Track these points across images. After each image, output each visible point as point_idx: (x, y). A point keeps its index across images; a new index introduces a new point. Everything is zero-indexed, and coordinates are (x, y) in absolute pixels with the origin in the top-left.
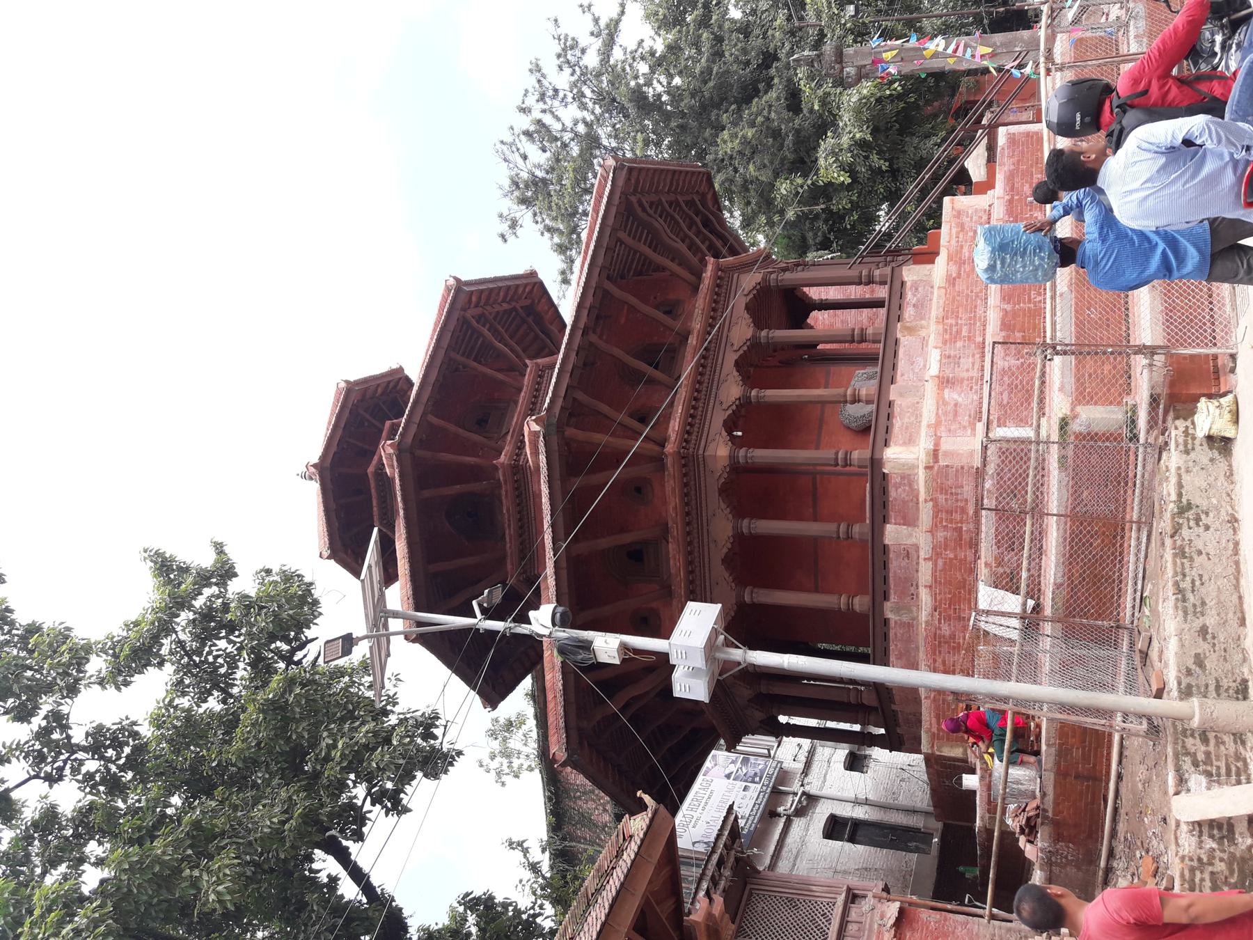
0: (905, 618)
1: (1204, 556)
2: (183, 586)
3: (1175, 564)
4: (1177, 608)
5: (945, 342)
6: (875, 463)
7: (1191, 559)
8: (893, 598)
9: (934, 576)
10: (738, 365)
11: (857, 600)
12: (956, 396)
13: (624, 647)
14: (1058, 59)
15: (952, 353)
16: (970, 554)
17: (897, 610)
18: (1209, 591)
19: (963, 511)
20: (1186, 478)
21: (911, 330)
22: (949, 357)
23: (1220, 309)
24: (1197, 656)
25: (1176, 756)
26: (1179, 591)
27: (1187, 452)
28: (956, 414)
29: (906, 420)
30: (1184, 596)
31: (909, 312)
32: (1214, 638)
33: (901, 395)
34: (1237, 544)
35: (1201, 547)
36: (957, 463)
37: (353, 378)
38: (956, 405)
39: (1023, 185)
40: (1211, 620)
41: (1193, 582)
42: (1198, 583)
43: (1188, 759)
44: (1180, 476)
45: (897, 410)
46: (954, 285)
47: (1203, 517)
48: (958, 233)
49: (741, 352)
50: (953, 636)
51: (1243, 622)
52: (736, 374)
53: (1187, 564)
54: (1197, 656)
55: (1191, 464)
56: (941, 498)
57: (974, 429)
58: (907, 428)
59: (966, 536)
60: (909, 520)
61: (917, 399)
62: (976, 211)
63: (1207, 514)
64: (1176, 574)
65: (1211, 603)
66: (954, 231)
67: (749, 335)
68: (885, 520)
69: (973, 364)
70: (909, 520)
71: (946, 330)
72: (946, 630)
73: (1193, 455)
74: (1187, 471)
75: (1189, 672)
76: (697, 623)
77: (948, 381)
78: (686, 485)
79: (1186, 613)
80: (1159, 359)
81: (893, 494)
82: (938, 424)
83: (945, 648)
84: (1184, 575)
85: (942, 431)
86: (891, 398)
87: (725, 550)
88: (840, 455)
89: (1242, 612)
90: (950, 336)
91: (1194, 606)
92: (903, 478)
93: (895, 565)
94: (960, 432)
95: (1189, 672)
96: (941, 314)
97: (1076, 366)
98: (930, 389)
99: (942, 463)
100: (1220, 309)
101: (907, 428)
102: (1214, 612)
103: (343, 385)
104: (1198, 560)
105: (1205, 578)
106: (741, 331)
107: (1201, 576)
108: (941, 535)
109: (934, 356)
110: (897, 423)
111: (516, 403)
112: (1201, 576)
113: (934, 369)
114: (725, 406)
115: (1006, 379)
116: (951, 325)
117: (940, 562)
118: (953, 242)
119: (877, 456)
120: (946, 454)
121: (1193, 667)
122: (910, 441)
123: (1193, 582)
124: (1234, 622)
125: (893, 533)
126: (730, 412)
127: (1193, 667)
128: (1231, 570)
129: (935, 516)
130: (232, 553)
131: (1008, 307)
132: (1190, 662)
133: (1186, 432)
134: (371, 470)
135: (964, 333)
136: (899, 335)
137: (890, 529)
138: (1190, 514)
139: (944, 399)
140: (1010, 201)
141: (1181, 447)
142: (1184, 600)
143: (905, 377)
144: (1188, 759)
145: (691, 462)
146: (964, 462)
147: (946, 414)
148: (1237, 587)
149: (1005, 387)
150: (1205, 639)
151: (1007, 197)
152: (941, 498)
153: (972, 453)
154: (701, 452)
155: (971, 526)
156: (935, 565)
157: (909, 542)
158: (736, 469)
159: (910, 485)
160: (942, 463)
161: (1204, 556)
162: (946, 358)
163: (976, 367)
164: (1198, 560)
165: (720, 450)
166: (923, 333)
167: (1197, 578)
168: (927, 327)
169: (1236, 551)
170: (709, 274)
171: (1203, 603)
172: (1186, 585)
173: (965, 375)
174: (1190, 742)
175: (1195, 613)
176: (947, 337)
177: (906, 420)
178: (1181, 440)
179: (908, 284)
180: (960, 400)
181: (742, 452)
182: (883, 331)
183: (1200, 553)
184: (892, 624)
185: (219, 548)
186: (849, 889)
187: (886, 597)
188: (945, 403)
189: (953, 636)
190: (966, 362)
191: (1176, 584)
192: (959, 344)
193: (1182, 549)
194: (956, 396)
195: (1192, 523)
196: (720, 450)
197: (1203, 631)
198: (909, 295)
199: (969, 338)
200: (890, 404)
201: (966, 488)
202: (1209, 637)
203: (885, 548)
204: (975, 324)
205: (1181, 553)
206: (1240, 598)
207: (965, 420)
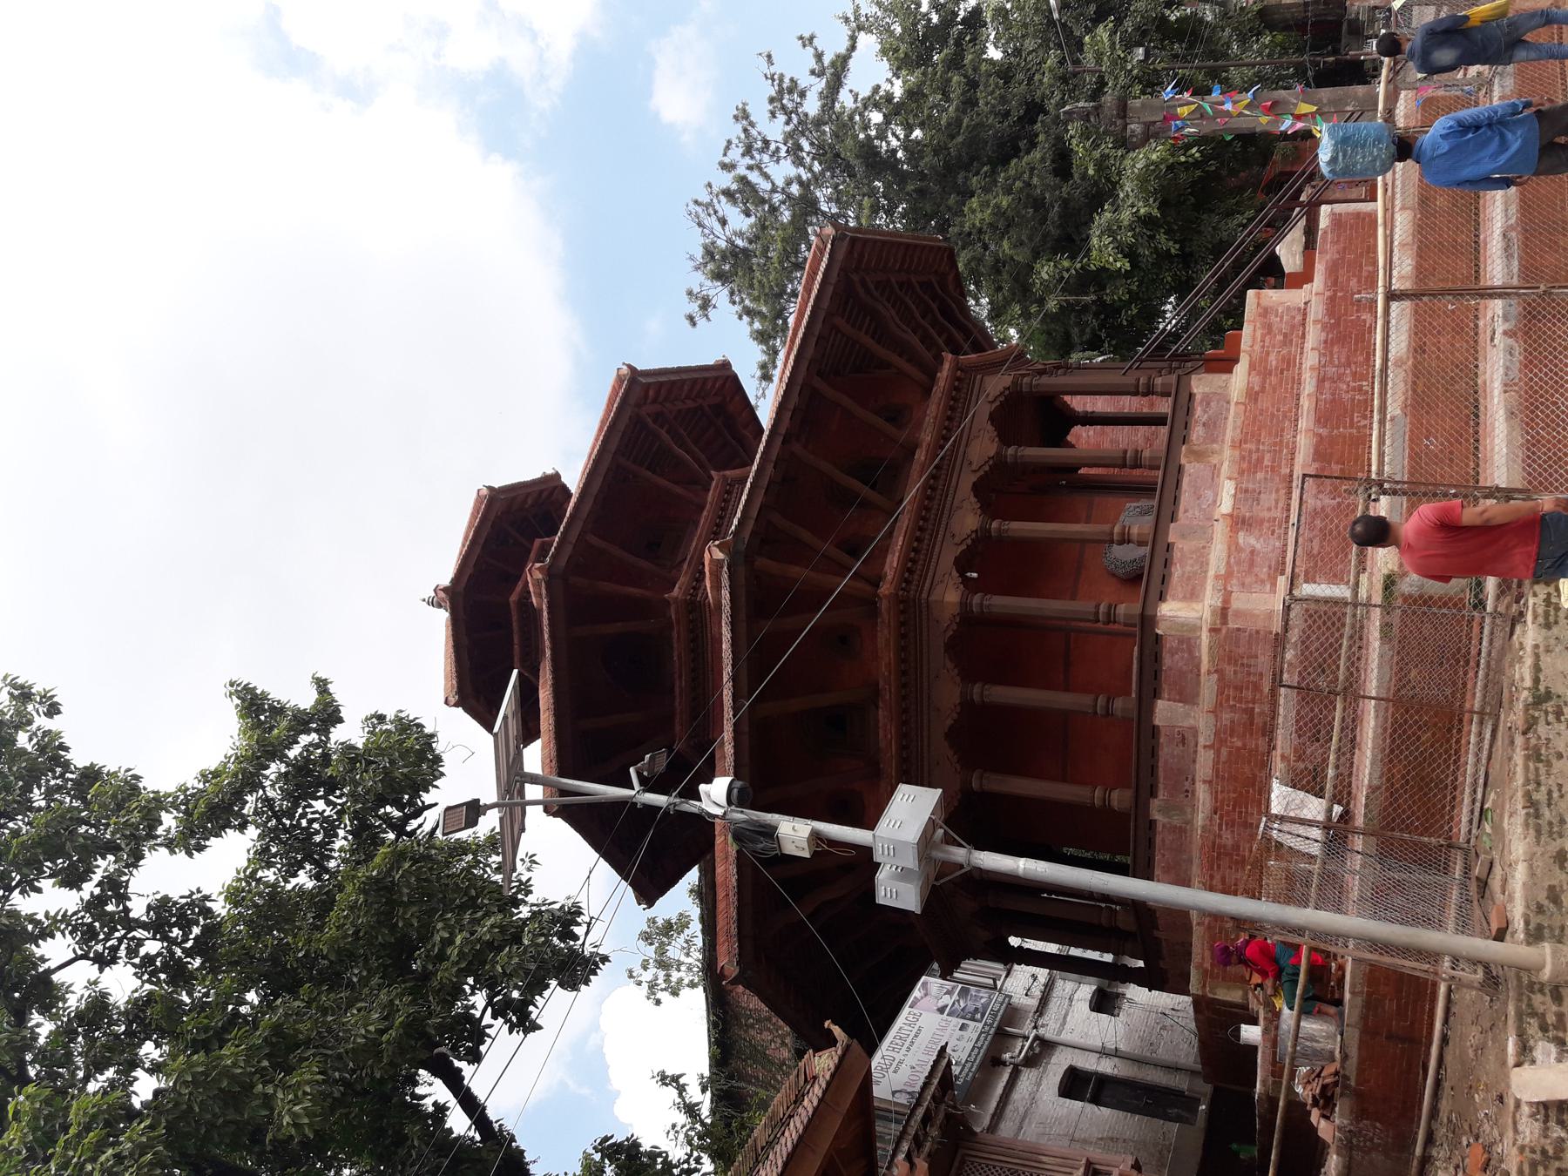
0: (1176, 821)
3: (1526, 768)
4: (1527, 825)
5: (1241, 473)
6: (1147, 621)
7: (1549, 764)
8: (1162, 794)
9: (1216, 762)
10: (976, 488)
11: (1115, 795)
12: (1252, 541)
13: (816, 836)
15: (1251, 486)
16: (1262, 743)
17: (1165, 810)
19: (1257, 687)
20: (1546, 660)
21: (1199, 456)
22: (1246, 491)
24: (1551, 888)
25: (1520, 1016)
26: (1531, 803)
27: (1548, 626)
28: (1252, 564)
29: (1188, 568)
30: (1537, 810)
31: (1197, 433)
33: (1183, 536)
36: (1251, 626)
38: (1252, 552)
39: (1349, 280)
41: (1550, 793)
42: (1556, 795)
43: (1534, 1022)
44: (1537, 656)
45: (1177, 554)
46: (1256, 400)
48: (1263, 336)
49: (981, 473)
50: (1236, 847)
52: (973, 499)
53: (1543, 770)
54: (1551, 888)
55: (1552, 641)
56: (1229, 670)
57: (1274, 584)
58: (1189, 578)
59: (1258, 721)
60: (1187, 696)
61: (1203, 543)
64: (1527, 781)
68: (1156, 694)
69: (1277, 502)
70: (1187, 696)
71: (1243, 458)
72: (1227, 838)
73: (1555, 630)
74: (1548, 651)
75: (1540, 909)
76: (910, 811)
77: (1243, 522)
79: (1538, 832)
81: (1167, 661)
82: (1228, 575)
83: (1225, 862)
84: (1539, 784)
85: (1234, 585)
86: (1171, 539)
87: (949, 722)
90: (1248, 466)
91: (1550, 824)
92: (1181, 641)
93: (1167, 752)
94: (1257, 587)
95: (1540, 909)
96: (1238, 436)
98: (1220, 531)
99: (1231, 625)
103: (485, 492)
104: (1557, 765)
106: (983, 446)
107: (1560, 786)
108: (1226, 716)
109: (1228, 489)
110: (1177, 572)
111: (696, 523)
112: (1560, 786)
113: (1226, 506)
114: (957, 540)
115: (1318, 522)
116: (1250, 452)
117: (1224, 751)
118: (1257, 348)
119: (1149, 612)
120: (1238, 614)
121: (1546, 903)
122: (1193, 595)
123: (1550, 793)
125: (1165, 711)
126: (964, 547)
127: (1546, 903)
129: (1220, 692)
130: (338, 692)
131: (1323, 431)
132: (1542, 897)
133: (1548, 601)
134: (513, 598)
135: (1266, 463)
136: (1183, 461)
137: (1161, 705)
138: (1549, 706)
140: (1332, 299)
141: (1541, 620)
142: (1537, 816)
143: (1189, 514)
144: (1534, 1022)
145: (911, 608)
146: (1260, 625)
147: (1238, 563)
149: (1316, 532)
151: (1328, 294)
152: (1229, 670)
153: (1270, 615)
154: (924, 595)
156: (1218, 754)
157: (1186, 724)
158: (969, 620)
159: (1190, 652)
160: (1231, 625)
162: (1242, 493)
163: (1280, 505)
164: (1557, 765)
165: (949, 595)
166: (1214, 460)
167: (1555, 789)
172: (1540, 796)
173: (1266, 515)
174: (1537, 999)
175: (1551, 833)
176: (1245, 466)
177: (1188, 568)
178: (1540, 611)
179: (1198, 398)
180: (1258, 546)
182: (1163, 455)
184: (1159, 828)
185: (322, 685)
186: (1089, 1164)
187: (1153, 793)
188: (1239, 549)
189: (1236, 847)
190: (1268, 499)
191: (1528, 795)
192: (1260, 476)
193: (1537, 750)
194: (1252, 541)
195: (1551, 718)
196: (949, 595)
200: (1169, 547)
201: (1261, 659)
203: (1155, 731)
204: (1281, 451)
205: (1534, 755)
207: (1263, 572)
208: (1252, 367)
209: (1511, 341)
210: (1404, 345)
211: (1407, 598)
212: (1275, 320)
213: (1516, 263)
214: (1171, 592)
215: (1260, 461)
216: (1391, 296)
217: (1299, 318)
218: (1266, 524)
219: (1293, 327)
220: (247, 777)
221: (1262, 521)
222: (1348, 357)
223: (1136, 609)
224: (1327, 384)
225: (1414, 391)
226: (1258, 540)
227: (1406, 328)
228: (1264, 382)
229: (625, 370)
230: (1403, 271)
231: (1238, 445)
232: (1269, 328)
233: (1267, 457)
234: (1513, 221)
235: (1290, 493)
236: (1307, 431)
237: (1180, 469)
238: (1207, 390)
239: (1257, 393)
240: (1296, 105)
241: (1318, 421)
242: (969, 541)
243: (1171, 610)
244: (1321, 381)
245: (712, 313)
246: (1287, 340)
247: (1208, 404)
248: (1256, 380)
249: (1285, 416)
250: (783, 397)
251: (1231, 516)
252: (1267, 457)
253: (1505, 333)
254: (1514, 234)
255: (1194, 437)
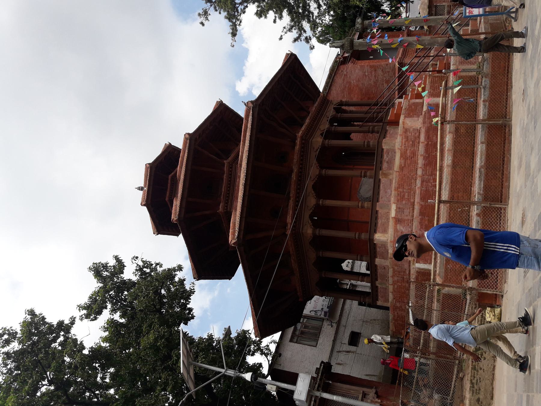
0: (384, 286)
1: (482, 370)
2: (107, 286)
3: (471, 372)
4: (470, 390)
5: (398, 201)
7: (478, 371)
9: (393, 289)
10: (314, 187)
12: (402, 228)
14: (448, 119)
15: (401, 206)
18: (482, 385)
19: (404, 272)
22: (400, 208)
23: (501, 274)
26: (472, 383)
29: (383, 221)
30: (473, 385)
31: (385, 165)
32: (482, 403)
33: (381, 208)
34: (494, 367)
35: (481, 366)
37: (151, 161)
39: (433, 136)
40: (481, 397)
41: (477, 380)
42: (479, 381)
45: (379, 215)
46: (403, 170)
47: (484, 354)
48: (405, 142)
51: (492, 398)
52: (313, 192)
53: (476, 373)
56: (396, 268)
58: (383, 225)
59: (405, 280)
61: (387, 211)
62: (414, 129)
63: (485, 353)
64: (471, 376)
65: (482, 390)
66: (404, 140)
67: (318, 173)
68: (375, 257)
69: (409, 213)
71: (398, 194)
72: (398, 305)
77: (399, 221)
78: (302, 160)
80: (474, 292)
81: (378, 249)
84: (474, 377)
87: (313, 261)
88: (360, 205)
89: (493, 394)
90: (400, 198)
92: (382, 245)
96: (397, 186)
97: (446, 264)
98: (391, 223)
100: (501, 274)
101: (383, 225)
102: (483, 393)
103: (148, 166)
104: (481, 372)
105: (482, 379)
107: (480, 378)
109: (394, 207)
110: (380, 222)
111: (223, 179)
112: (480, 378)
113: (393, 214)
116: (401, 192)
117: (396, 286)
118: (403, 147)
122: (385, 231)
123: (477, 380)
124: (489, 397)
126: (311, 211)
128: (491, 377)
130: (122, 257)
134: (170, 176)
135: (406, 197)
136: (380, 178)
139: (397, 229)
141: (479, 322)
142: (473, 387)
143: (383, 199)
145: (297, 234)
148: (492, 384)
150: (478, 403)
151: (426, 143)
152: (396, 268)
154: (301, 231)
155: (408, 277)
156: (394, 286)
159: (385, 248)
161: (482, 370)
162: (399, 210)
164: (481, 372)
165: (309, 231)
166: (390, 177)
167: (479, 379)
168: (392, 174)
169: (494, 369)
170: (298, 147)
171: (480, 389)
172: (474, 381)
173: (406, 218)
175: (476, 393)
176: (399, 198)
177: (383, 221)
178: (480, 319)
179: (385, 150)
180: (404, 230)
181: (323, 172)
183: (481, 369)
184: (379, 288)
185: (117, 258)
187: (377, 280)
190: (407, 212)
191: (471, 381)
192: (404, 202)
194: (402, 228)
196: (309, 231)
197: (478, 400)
198: (385, 156)
199: (408, 199)
200: (377, 212)
201: (405, 266)
202: (480, 402)
203: (376, 266)
204: (411, 192)
206: (493, 388)
208: (401, 156)
209: (478, 218)
210: (447, 196)
211: (444, 294)
212: (409, 134)
213: (483, 183)
214: (378, 230)
215: (404, 196)
216: (440, 202)
217: (417, 134)
218: (406, 222)
219: (415, 138)
220: (104, 290)
221: (404, 221)
222: (432, 172)
223: (367, 236)
224: (424, 183)
225: (449, 216)
226: (403, 228)
227: (448, 189)
228: (405, 163)
229: (187, 136)
230: (445, 196)
231: (397, 189)
232: (407, 138)
233: (406, 194)
234: (483, 164)
235: (413, 210)
236: (418, 203)
237: (380, 180)
238: (388, 147)
239: (403, 167)
240: (416, 45)
241: (421, 199)
242: (313, 209)
243: (378, 237)
244: (422, 182)
245: (209, 17)
246: (413, 145)
247: (388, 153)
248: (403, 161)
249: (412, 177)
250: (243, 198)
251: (395, 218)
252: (406, 194)
253: (477, 214)
254: (483, 170)
255: (384, 167)
